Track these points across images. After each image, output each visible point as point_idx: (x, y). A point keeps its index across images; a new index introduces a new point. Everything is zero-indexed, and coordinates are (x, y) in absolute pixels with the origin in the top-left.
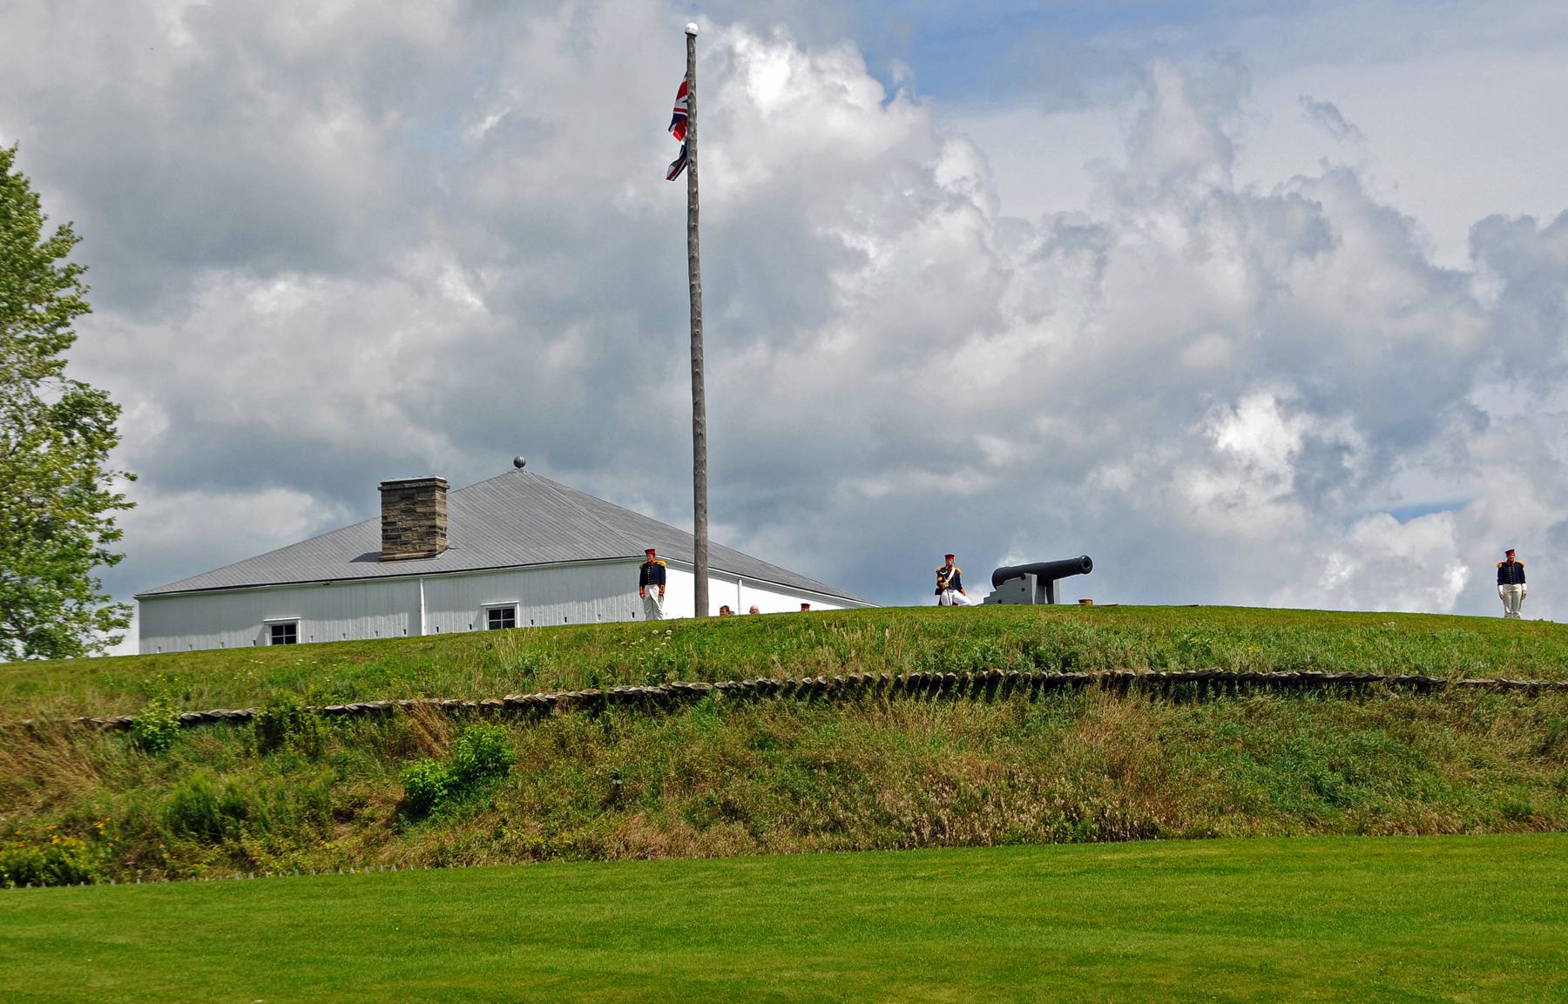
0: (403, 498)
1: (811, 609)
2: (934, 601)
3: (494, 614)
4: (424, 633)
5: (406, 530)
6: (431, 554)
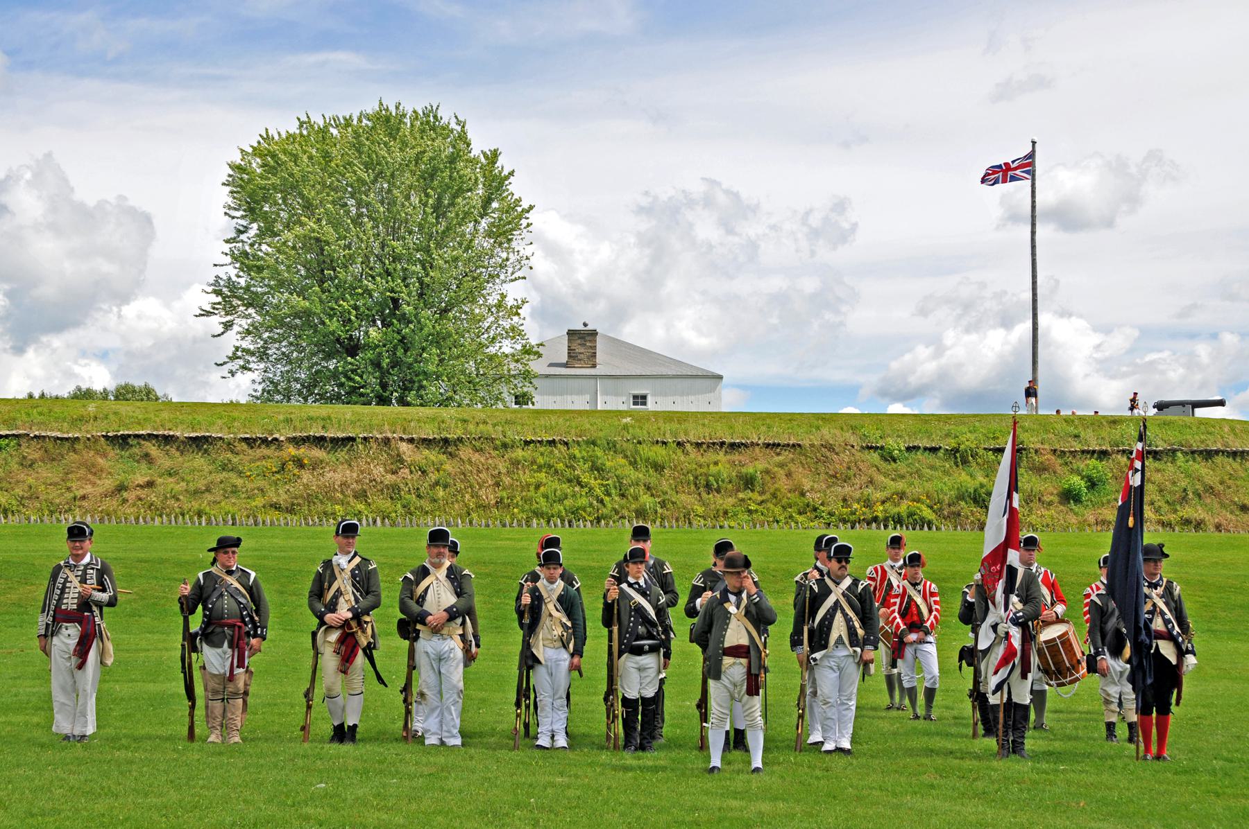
2: (1129, 413)
3: (635, 397)
4: (599, 409)
5: (580, 353)
6: (594, 366)
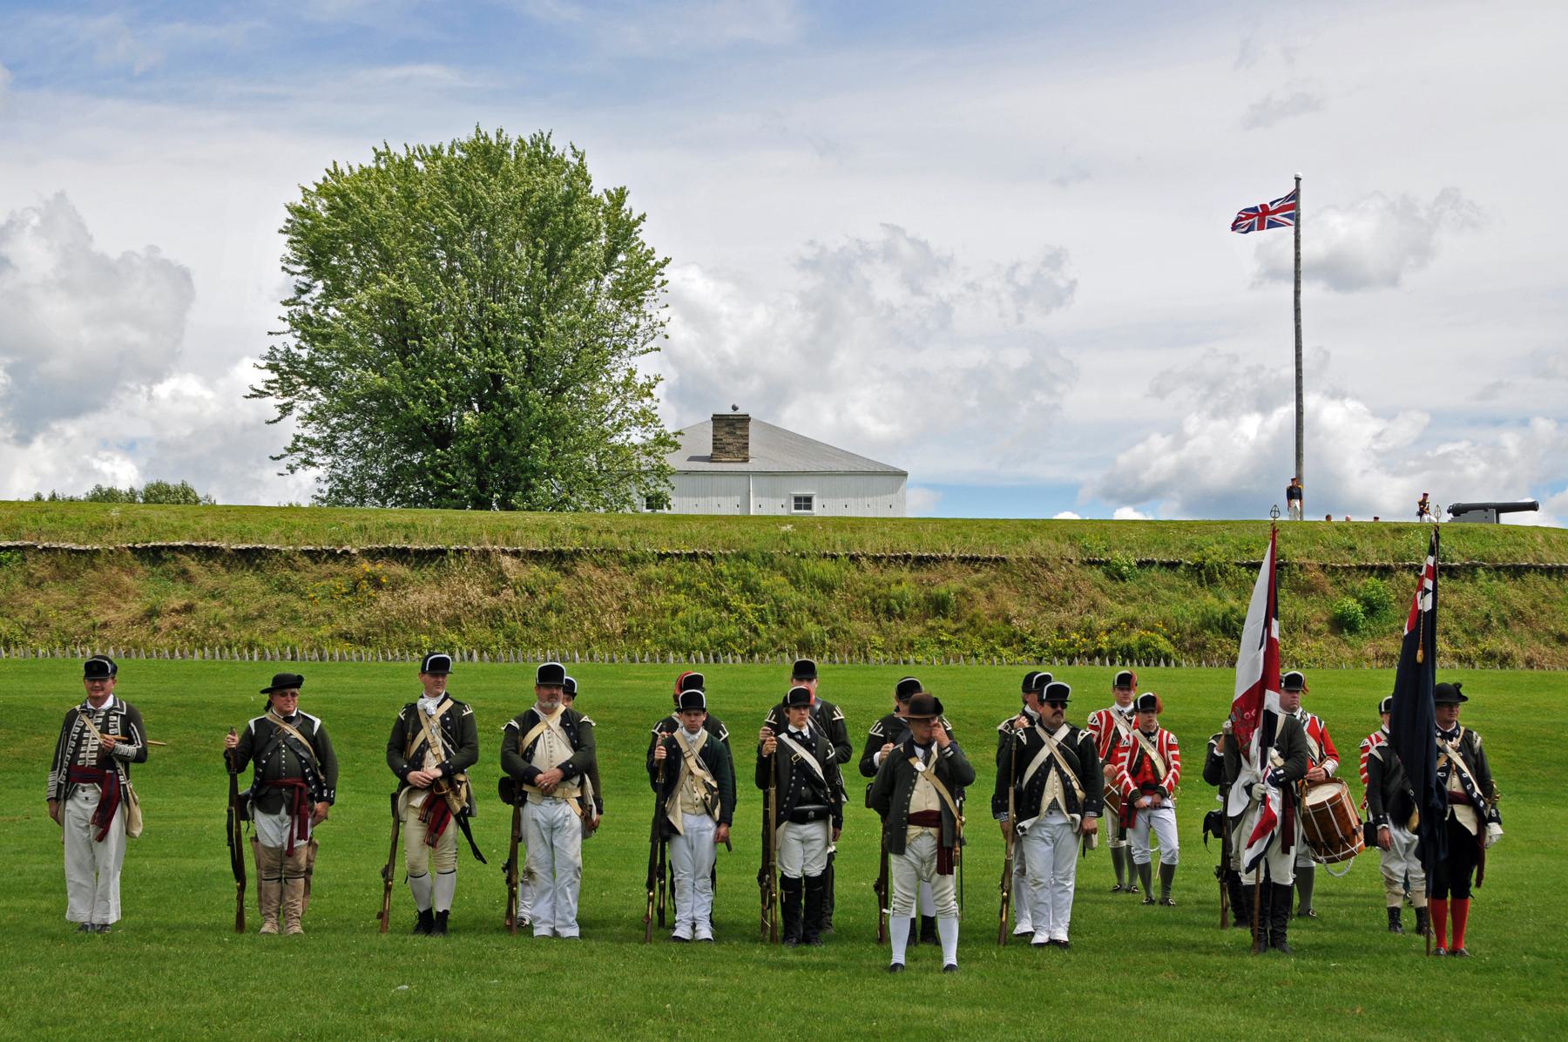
0: (727, 425)
1: (817, 510)
3: (797, 499)
4: (752, 513)
5: (729, 444)
6: (746, 460)
